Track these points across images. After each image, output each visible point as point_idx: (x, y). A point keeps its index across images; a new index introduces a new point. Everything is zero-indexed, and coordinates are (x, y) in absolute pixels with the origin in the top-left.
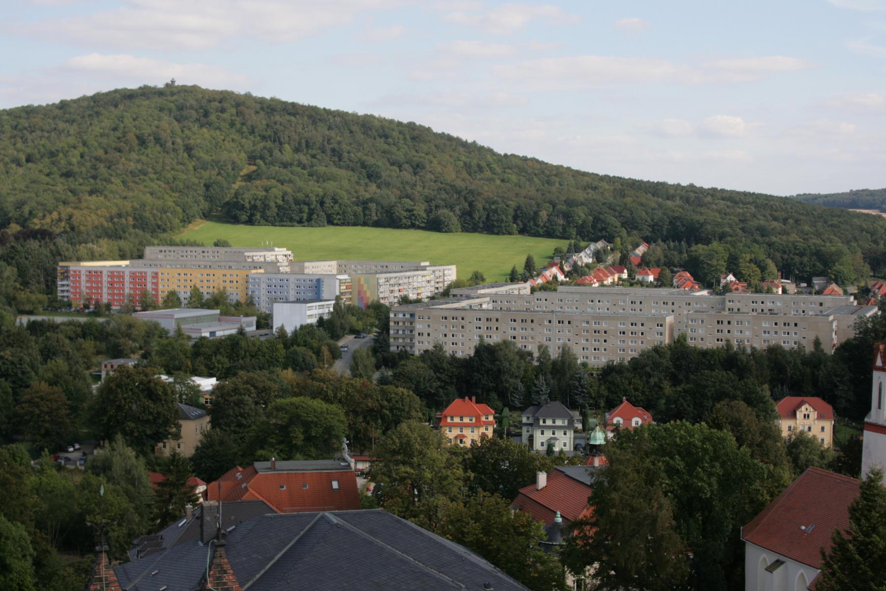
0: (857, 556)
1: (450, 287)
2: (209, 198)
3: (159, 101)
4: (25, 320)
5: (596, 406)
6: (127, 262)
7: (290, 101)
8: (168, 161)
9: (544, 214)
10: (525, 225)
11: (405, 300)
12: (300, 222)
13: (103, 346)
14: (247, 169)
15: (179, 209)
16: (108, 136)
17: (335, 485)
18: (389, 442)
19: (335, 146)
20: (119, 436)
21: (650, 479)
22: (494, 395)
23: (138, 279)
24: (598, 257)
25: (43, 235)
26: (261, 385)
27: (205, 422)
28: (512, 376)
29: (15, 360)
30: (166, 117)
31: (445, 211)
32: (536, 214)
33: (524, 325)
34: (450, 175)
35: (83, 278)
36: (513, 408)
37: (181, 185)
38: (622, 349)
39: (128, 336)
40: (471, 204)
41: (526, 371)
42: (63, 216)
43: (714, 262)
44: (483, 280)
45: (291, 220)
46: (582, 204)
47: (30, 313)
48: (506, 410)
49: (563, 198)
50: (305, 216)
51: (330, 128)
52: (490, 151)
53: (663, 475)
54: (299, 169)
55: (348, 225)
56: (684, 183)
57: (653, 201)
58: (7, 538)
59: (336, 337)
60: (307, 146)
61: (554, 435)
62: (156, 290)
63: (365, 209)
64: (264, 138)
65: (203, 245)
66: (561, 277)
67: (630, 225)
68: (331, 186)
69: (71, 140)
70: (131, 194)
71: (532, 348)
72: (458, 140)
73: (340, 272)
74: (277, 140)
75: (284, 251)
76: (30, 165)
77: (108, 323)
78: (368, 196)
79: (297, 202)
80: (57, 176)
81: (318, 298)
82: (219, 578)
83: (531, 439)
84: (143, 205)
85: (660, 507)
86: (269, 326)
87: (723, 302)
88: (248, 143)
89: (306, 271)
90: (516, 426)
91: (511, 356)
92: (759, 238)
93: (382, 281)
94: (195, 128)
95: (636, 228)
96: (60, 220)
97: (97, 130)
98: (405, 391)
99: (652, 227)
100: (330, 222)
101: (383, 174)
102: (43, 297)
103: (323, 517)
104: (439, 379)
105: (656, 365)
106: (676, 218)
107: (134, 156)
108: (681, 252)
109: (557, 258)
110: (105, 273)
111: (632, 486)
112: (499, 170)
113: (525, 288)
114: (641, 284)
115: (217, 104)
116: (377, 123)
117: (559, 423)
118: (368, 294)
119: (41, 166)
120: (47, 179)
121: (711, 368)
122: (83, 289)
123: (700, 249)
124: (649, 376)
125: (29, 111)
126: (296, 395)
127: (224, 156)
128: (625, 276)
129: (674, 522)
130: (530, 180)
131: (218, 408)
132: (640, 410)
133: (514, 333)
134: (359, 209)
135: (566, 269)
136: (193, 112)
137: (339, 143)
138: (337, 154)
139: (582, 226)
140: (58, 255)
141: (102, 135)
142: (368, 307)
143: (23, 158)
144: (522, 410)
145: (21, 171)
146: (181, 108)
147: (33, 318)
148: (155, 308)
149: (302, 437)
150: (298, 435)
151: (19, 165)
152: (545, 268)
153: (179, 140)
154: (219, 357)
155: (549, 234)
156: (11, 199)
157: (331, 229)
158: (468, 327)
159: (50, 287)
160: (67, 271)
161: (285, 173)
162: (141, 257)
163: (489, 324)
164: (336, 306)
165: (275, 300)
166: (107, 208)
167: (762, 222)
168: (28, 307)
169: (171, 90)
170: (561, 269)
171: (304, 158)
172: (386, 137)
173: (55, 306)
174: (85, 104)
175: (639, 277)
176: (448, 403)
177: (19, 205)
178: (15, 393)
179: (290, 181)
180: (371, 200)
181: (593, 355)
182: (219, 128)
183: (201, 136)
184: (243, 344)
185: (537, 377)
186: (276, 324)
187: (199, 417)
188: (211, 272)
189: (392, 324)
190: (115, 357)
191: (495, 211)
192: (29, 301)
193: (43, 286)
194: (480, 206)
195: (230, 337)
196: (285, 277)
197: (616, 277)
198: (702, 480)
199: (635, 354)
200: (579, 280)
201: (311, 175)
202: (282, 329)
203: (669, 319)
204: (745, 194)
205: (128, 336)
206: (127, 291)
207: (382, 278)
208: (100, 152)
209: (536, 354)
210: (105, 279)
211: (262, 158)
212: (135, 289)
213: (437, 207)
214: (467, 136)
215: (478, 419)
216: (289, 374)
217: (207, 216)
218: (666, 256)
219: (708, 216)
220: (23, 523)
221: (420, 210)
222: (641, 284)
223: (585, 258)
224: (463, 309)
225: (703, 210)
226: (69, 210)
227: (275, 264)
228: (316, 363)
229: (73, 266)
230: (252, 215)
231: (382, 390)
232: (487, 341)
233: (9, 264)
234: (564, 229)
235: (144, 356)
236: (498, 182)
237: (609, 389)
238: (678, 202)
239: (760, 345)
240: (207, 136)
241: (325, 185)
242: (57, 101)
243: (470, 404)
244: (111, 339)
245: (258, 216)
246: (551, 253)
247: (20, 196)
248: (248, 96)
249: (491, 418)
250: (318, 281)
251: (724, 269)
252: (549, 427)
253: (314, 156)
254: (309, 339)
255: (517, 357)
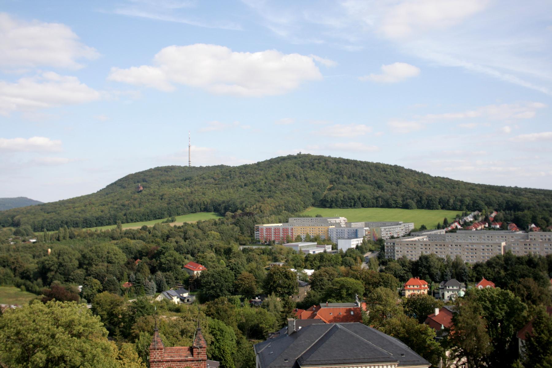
0: (535, 343)
1: (411, 232)
2: (314, 198)
3: (295, 160)
4: (241, 248)
5: (472, 281)
6: (281, 224)
7: (346, 158)
8: (298, 184)
9: (451, 201)
10: (444, 206)
11: (392, 237)
12: (351, 207)
13: (271, 257)
14: (329, 186)
15: (302, 203)
16: (275, 175)
17: (352, 313)
18: (373, 295)
19: (364, 175)
20: (273, 293)
21: (476, 310)
22: (428, 276)
23: (285, 230)
24: (475, 217)
25: (250, 214)
26: (330, 273)
27: (308, 288)
28: (435, 268)
29: (236, 263)
30: (297, 167)
31: (410, 201)
32: (448, 201)
33: (441, 247)
34: (412, 186)
35: (264, 231)
36: (436, 282)
37: (303, 193)
38: (483, 257)
39: (280, 253)
40: (421, 198)
41: (441, 266)
42: (258, 207)
43: (526, 219)
44: (426, 229)
45: (347, 206)
46: (468, 196)
47: (244, 245)
48: (433, 283)
49: (459, 194)
50: (353, 204)
51: (362, 169)
52: (429, 175)
53: (481, 309)
54: (350, 185)
55: (370, 207)
56: (513, 186)
57: (498, 194)
58: (226, 332)
59: (363, 253)
60: (353, 176)
61: (453, 292)
62: (292, 235)
63: (377, 200)
64: (336, 173)
65: (311, 217)
66: (459, 227)
67: (489, 204)
68: (363, 192)
69: (261, 177)
70: (284, 197)
71: (443, 256)
72: (415, 172)
73: (366, 227)
74: (341, 174)
75: (343, 218)
76: (246, 187)
77: (273, 248)
78: (378, 195)
79: (349, 199)
80: (255, 191)
81: (356, 237)
82: (198, 342)
83: (443, 295)
84: (288, 201)
85: (479, 323)
86: (336, 249)
87: (527, 236)
88: (329, 176)
89: (352, 226)
90: (437, 289)
91: (434, 260)
92: (546, 209)
93: (382, 230)
94: (309, 170)
95: (492, 205)
96: (257, 208)
97: (271, 173)
98: (390, 275)
99: (498, 205)
100: (363, 206)
101: (384, 186)
102: (249, 239)
103: (335, 326)
104: (404, 270)
105: (497, 264)
106: (508, 201)
107: (285, 182)
108: (511, 215)
109: (457, 219)
110: (272, 229)
111: (468, 314)
112: (432, 183)
113: (443, 232)
114: (494, 229)
115: (317, 161)
116: (382, 166)
117: (455, 288)
118: (377, 235)
119: (250, 188)
120: (252, 192)
121: (522, 264)
122: (265, 235)
123: (520, 213)
124: (494, 268)
125: (245, 166)
126: (344, 276)
127: (320, 181)
128: (487, 225)
129: (486, 330)
130: (446, 187)
131: (313, 283)
132: (490, 283)
133: (437, 250)
134: (374, 201)
135: (461, 223)
136: (308, 165)
137: (366, 174)
138: (365, 179)
139: (468, 205)
140: (255, 222)
141: (273, 175)
142: (377, 241)
143: (243, 184)
144: (440, 282)
145: (242, 190)
146: (303, 163)
147: (245, 247)
148: (292, 242)
149: (345, 293)
150: (344, 292)
151: (242, 187)
152: (452, 223)
153: (302, 176)
154: (315, 261)
155: (454, 209)
156: (239, 200)
157: (363, 209)
158: (417, 248)
159: (252, 235)
160: (258, 228)
161: (344, 187)
162: (287, 222)
163: (426, 247)
164: (364, 241)
165: (339, 238)
166: (275, 203)
167: (547, 202)
168: (244, 242)
169: (300, 156)
170: (459, 223)
171: (352, 181)
172: (385, 171)
173: (255, 242)
174: (267, 163)
175: (493, 226)
176: (408, 279)
177: (241, 203)
178: (236, 276)
179: (347, 190)
180: (379, 197)
181: (469, 259)
182: (318, 170)
183: (311, 174)
184: (325, 256)
185: (446, 268)
186: (339, 248)
187: (307, 285)
188: (314, 227)
189: (385, 247)
190: (275, 262)
191: (431, 200)
192: (244, 240)
193: (250, 234)
194: (424, 198)
195: (320, 254)
196: (343, 229)
197: (483, 226)
198: (498, 312)
199: (489, 259)
200: (466, 227)
201: (355, 187)
202: (341, 250)
203: (503, 244)
204: (540, 190)
205: (280, 253)
206: (281, 235)
207: (383, 229)
208: (272, 181)
209: (446, 259)
210: (273, 231)
211: (335, 181)
212: (284, 235)
213: (407, 199)
214: (419, 170)
215: (420, 286)
216: (343, 268)
217: (313, 205)
218: (504, 217)
219: (523, 200)
220: (233, 326)
221: (400, 200)
222: (494, 229)
223: (470, 219)
224: (415, 241)
225: (521, 197)
226: (260, 204)
227: (339, 225)
228: (354, 263)
229: (260, 226)
230: (331, 204)
231: (380, 276)
232: (425, 253)
233: (236, 226)
234: (460, 207)
235: (286, 261)
236: (432, 188)
237: (477, 274)
238: (510, 194)
239: (543, 254)
240: (313, 173)
241: (360, 191)
242: (256, 162)
243: (418, 280)
244: (274, 254)
245: (334, 204)
246: (455, 217)
247: (242, 200)
248: (329, 157)
249: (426, 286)
250: (356, 230)
251: (530, 222)
252: (451, 290)
253: (356, 180)
254: (352, 254)
255: (437, 261)
